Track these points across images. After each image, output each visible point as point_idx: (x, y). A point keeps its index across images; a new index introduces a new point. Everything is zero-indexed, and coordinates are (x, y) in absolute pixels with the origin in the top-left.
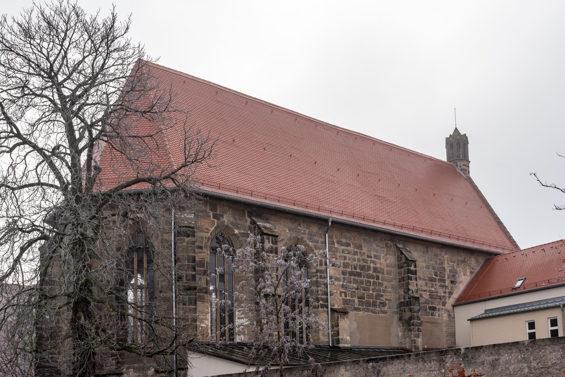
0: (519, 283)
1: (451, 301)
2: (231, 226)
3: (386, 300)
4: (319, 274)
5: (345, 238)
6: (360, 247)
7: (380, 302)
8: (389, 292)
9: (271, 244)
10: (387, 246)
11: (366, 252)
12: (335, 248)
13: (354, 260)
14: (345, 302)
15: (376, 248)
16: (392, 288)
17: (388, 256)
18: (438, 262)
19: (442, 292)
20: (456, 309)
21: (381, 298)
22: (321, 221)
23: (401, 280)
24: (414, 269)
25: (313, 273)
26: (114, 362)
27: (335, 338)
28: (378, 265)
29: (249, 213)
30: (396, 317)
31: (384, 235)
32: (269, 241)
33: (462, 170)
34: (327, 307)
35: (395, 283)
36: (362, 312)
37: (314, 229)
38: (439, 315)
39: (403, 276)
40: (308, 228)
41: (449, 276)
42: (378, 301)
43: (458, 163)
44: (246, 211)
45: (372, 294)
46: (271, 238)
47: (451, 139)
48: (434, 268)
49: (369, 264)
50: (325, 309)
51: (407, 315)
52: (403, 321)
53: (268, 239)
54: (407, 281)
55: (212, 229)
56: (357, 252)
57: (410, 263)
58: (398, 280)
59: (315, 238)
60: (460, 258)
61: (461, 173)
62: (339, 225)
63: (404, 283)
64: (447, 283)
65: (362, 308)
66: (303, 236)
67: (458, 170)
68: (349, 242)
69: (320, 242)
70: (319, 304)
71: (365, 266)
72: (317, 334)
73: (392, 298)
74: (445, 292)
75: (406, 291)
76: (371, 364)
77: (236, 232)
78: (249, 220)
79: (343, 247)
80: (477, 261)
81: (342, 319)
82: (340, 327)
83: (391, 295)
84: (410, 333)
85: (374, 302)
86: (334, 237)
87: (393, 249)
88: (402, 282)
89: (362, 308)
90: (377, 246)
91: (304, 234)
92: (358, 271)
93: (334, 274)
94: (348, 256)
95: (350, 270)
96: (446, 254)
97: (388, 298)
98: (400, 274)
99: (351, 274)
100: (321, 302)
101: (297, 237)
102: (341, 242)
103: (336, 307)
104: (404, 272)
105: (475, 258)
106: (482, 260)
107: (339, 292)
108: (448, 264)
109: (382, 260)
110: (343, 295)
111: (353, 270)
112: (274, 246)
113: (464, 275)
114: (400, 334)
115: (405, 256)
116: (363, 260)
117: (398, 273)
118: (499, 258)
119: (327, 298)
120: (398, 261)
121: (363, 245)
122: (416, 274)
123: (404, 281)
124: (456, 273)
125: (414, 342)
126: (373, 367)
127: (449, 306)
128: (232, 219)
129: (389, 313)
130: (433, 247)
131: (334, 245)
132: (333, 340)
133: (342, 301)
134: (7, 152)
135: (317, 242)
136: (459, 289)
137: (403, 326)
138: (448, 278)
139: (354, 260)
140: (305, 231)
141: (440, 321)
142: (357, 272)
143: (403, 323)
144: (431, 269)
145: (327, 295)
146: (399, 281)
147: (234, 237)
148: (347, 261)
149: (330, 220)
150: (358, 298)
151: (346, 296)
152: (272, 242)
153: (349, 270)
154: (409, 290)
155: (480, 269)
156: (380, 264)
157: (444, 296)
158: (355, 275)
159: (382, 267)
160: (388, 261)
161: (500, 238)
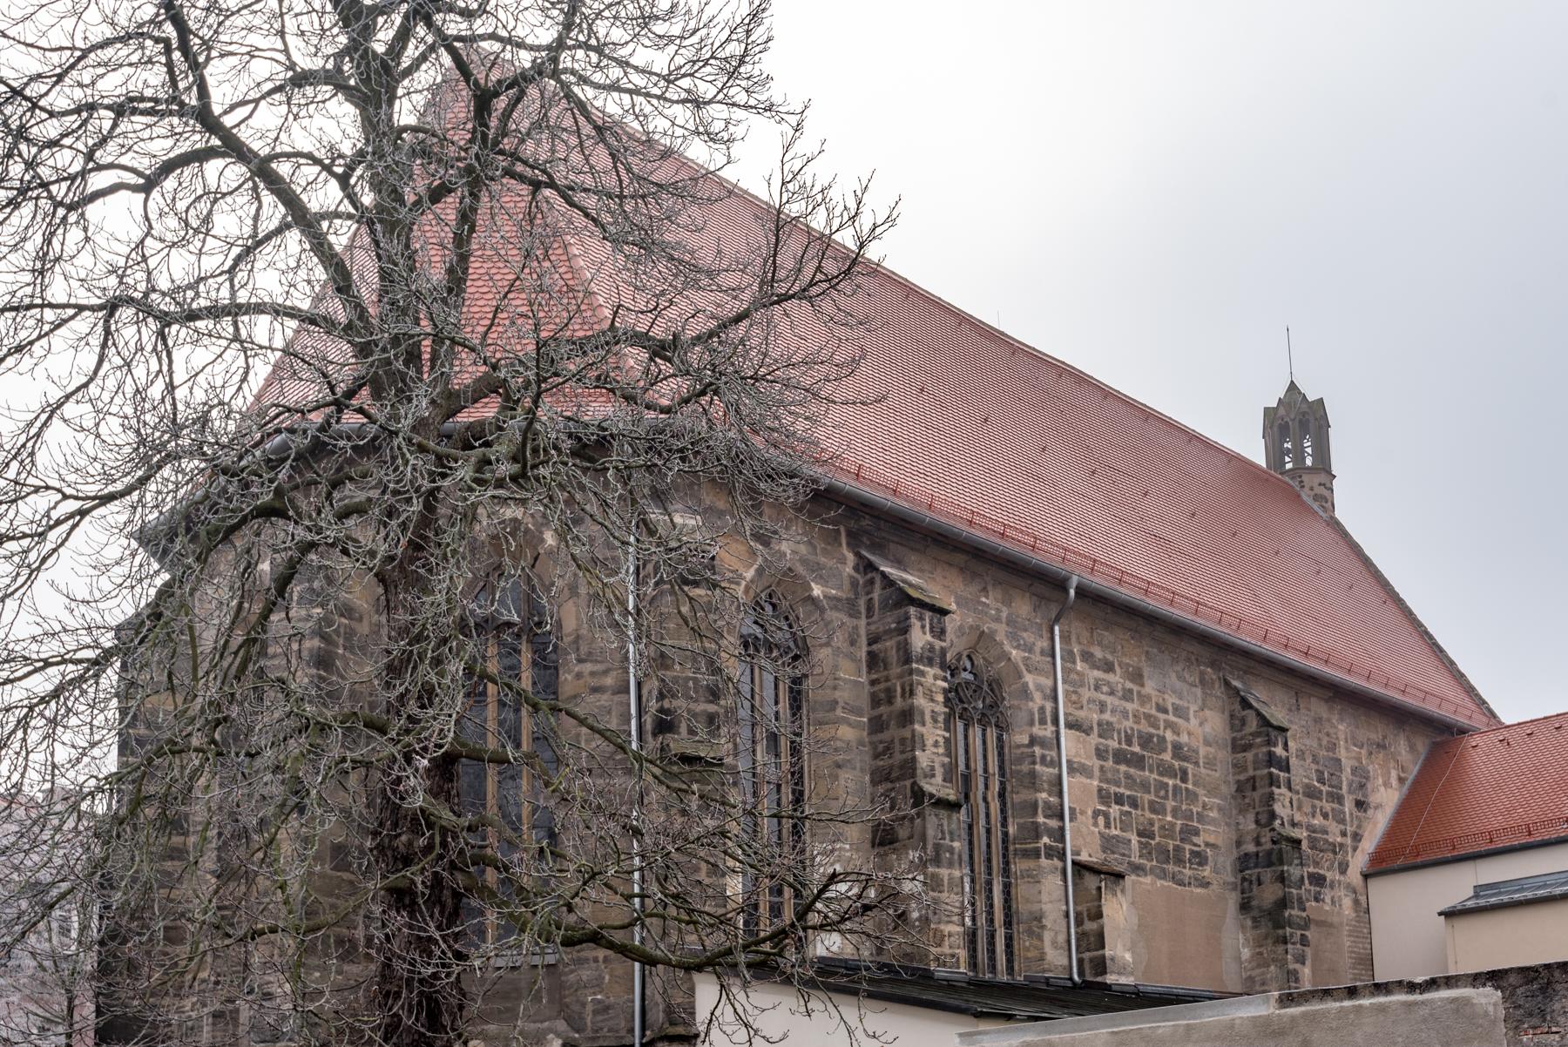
1: (1358, 861)
2: (800, 569)
3: (1207, 844)
4: (1037, 750)
5: (1100, 644)
6: (1137, 677)
7: (1192, 852)
8: (1213, 822)
9: (928, 637)
10: (1203, 682)
11: (1154, 693)
12: (1078, 673)
13: (1125, 714)
14: (1108, 844)
15: (1179, 685)
17: (1208, 713)
18: (1324, 743)
19: (1338, 832)
21: (1195, 840)
23: (1245, 787)
24: (1284, 754)
25: (1019, 746)
27: (1087, 955)
28: (1184, 739)
29: (850, 534)
30: (1233, 900)
31: (1196, 648)
32: (923, 627)
33: (1317, 498)
34: (1062, 856)
36: (1148, 880)
37: (1023, 607)
38: (1333, 902)
39: (1251, 773)
40: (1007, 602)
41: (1350, 785)
42: (1188, 847)
43: (1305, 478)
44: (842, 529)
45: (1173, 825)
46: (928, 615)
47: (1282, 412)
48: (1315, 760)
49: (1161, 732)
50: (1057, 862)
51: (1269, 894)
52: (1255, 913)
53: (921, 619)
54: (1267, 790)
55: (750, 574)
56: (1131, 691)
57: (1273, 733)
58: (1233, 788)
59: (1025, 635)
60: (1373, 736)
61: (1315, 506)
63: (1257, 795)
64: (1348, 806)
65: (1149, 865)
66: (994, 626)
67: (1306, 496)
68: (1110, 657)
69: (1037, 649)
70: (1041, 844)
71: (1151, 736)
72: (1035, 942)
73: (1219, 842)
74: (1344, 834)
75: (1264, 819)
77: (817, 591)
78: (850, 557)
79: (1097, 674)
80: (1412, 748)
81: (1109, 896)
82: (1105, 920)
83: (1218, 832)
84: (1281, 948)
85: (1177, 849)
86: (1074, 639)
87: (1218, 690)
89: (1149, 865)
90: (1179, 678)
91: (998, 620)
92: (1136, 749)
93: (1077, 755)
94: (1109, 700)
95: (1116, 745)
96: (1341, 720)
97: (1212, 840)
98: (1239, 767)
99: (1120, 757)
100: (1046, 840)
101: (978, 627)
103: (1084, 857)
104: (1255, 762)
105: (1408, 739)
106: (1422, 746)
107: (1090, 813)
109: (1194, 722)
110: (1101, 820)
111: (1124, 746)
112: (938, 644)
114: (1246, 953)
115: (1259, 714)
116: (1148, 717)
117: (1235, 766)
119: (1062, 829)
120: (1232, 727)
121: (1146, 672)
122: (1288, 770)
123: (1254, 789)
124: (1367, 778)
127: (1354, 875)
128: (803, 549)
129: (1215, 887)
130: (1310, 696)
131: (1074, 662)
132: (1080, 962)
133: (1098, 841)
134: (135, 189)
135: (1030, 650)
136: (1375, 825)
137: (1255, 927)
138: (1349, 792)
139: (1125, 716)
140: (998, 610)
141: (1335, 920)
142: (1133, 754)
143: (1254, 920)
144: (1309, 760)
145: (1061, 818)
147: (810, 607)
148: (1107, 716)
149: (1075, 580)
150: (1139, 835)
151: (1107, 826)
152: (932, 631)
153: (1113, 744)
154: (1273, 816)
155: (1420, 772)
156: (1189, 734)
157: (1341, 845)
158: (1128, 763)
159: (1194, 744)
160: (1207, 728)
161: (1442, 684)
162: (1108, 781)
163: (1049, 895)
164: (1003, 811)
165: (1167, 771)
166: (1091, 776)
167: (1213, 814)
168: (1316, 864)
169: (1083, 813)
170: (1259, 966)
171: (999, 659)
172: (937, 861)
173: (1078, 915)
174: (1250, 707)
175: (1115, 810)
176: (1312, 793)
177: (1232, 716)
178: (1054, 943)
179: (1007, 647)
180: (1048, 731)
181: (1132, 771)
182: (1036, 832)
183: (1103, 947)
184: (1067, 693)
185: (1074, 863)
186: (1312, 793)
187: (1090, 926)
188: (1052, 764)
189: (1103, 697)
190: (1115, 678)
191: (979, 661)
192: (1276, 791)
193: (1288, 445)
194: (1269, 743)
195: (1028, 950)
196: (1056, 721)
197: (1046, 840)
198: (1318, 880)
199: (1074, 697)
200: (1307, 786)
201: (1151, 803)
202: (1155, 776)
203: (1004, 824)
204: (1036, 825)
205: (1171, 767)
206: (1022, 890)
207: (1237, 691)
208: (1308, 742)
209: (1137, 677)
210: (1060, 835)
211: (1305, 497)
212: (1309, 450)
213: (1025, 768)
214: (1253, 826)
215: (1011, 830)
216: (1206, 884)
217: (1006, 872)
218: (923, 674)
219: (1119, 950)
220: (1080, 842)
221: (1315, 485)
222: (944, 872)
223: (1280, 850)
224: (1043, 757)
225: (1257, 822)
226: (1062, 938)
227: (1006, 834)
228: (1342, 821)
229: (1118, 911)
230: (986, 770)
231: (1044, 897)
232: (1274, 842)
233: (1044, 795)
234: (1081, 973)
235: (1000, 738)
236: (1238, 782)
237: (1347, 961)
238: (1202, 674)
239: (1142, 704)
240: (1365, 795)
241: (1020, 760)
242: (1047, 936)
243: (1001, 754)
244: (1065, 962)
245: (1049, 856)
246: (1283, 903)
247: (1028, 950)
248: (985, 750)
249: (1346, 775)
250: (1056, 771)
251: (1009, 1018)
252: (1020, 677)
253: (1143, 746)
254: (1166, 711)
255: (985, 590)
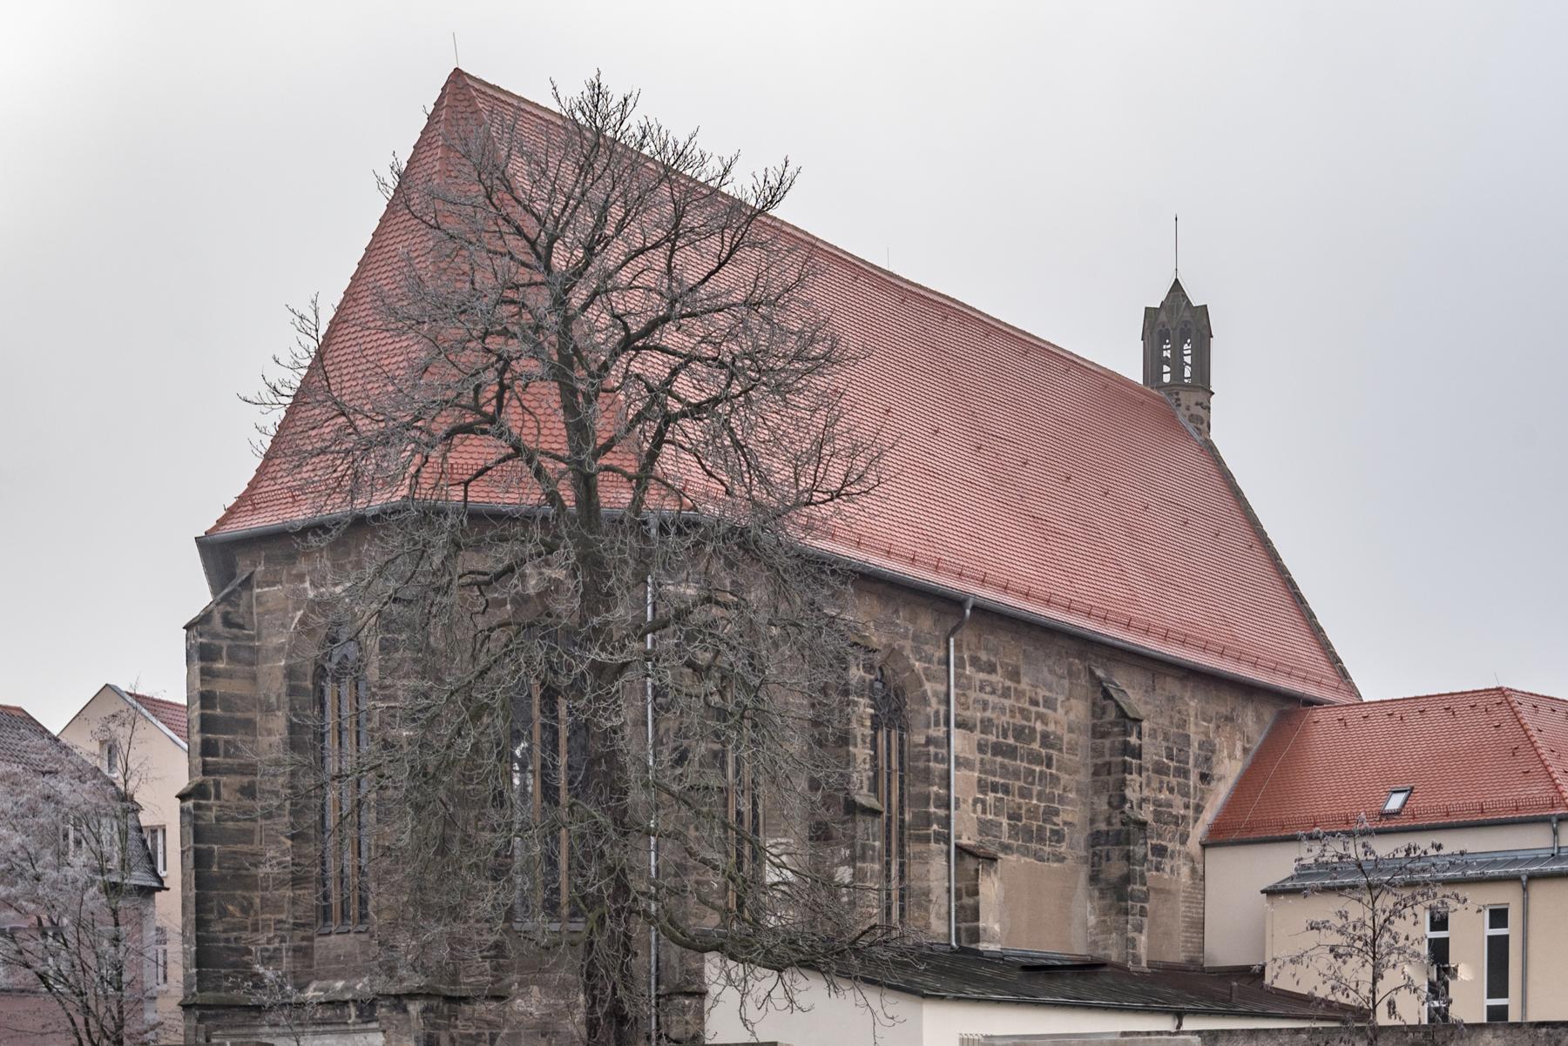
0: (1395, 802)
1: (1198, 832)
3: (1065, 823)
4: (932, 749)
5: (986, 649)
6: (1015, 675)
7: (1052, 831)
10: (1071, 674)
11: (1028, 688)
13: (1003, 710)
14: (985, 827)
15: (1049, 678)
16: (1078, 791)
20: (1210, 853)
21: (1055, 819)
22: (946, 604)
25: (917, 745)
26: (487, 964)
27: (963, 925)
28: (1051, 728)
30: (1083, 873)
33: (1192, 418)
34: (947, 841)
35: (1084, 777)
37: (926, 623)
38: (1172, 871)
39: (1107, 758)
40: (913, 621)
41: (1196, 760)
43: (1182, 395)
45: (1037, 807)
48: (1166, 739)
50: (943, 846)
51: (1115, 869)
52: (1102, 885)
54: (1120, 776)
57: (1129, 724)
58: (1091, 770)
59: (926, 647)
62: (991, 617)
63: (1111, 779)
64: (1194, 779)
66: (902, 642)
67: (1182, 417)
68: (993, 659)
69: (935, 659)
71: (1024, 727)
73: (1076, 821)
74: (1187, 807)
76: (1544, 1030)
79: (982, 676)
80: (1259, 719)
84: (1122, 919)
85: (1040, 829)
87: (1084, 680)
88: (1104, 777)
91: (905, 637)
92: (1011, 741)
93: (963, 750)
94: (991, 699)
96: (1193, 697)
97: (1069, 818)
98: (1097, 751)
99: (998, 749)
100: (935, 827)
102: (978, 659)
103: (964, 841)
106: (1269, 714)
108: (1196, 724)
109: (1060, 711)
110: (979, 807)
113: (1230, 757)
114: (1092, 920)
115: (1118, 705)
116: (1022, 710)
117: (1093, 750)
118: (1319, 714)
119: (948, 817)
120: (1094, 715)
122: (1140, 757)
123: (1109, 773)
124: (1213, 752)
125: (1132, 943)
126: (1547, 1034)
127: (1193, 845)
129: (1069, 862)
130: (1166, 675)
132: (958, 930)
135: (930, 661)
141: (1173, 887)
142: (1009, 745)
143: (1101, 891)
144: (1160, 738)
145: (948, 807)
146: (1095, 774)
148: (988, 714)
151: (984, 812)
153: (992, 738)
154: (1124, 799)
157: (1184, 817)
158: (1004, 754)
160: (1072, 716)
162: (986, 772)
163: (936, 873)
164: (901, 801)
165: (1034, 758)
166: (973, 770)
167: (1072, 795)
168: (1160, 836)
169: (965, 801)
170: (1103, 932)
171: (904, 670)
172: (863, 858)
173: (958, 890)
174: (1111, 697)
175: (990, 797)
176: (1160, 769)
177: (1094, 704)
178: (938, 915)
179: (912, 661)
180: (939, 732)
181: (1006, 761)
182: (927, 820)
183: (977, 919)
184: (957, 695)
185: (957, 846)
186: (1160, 769)
187: (967, 901)
188: (942, 761)
189: (986, 697)
190: (997, 678)
191: (887, 672)
192: (1128, 777)
193: (1167, 354)
194: (1126, 733)
195: (916, 919)
196: (947, 723)
197: (935, 827)
198: (1160, 851)
199: (963, 700)
200: (1157, 763)
201: (1021, 788)
202: (1025, 764)
203: (902, 813)
204: (928, 814)
205: (1039, 755)
206: (914, 869)
207: (1099, 681)
208: (1160, 721)
209: (1015, 675)
210: (946, 822)
211: (1180, 418)
212: (1188, 359)
213: (921, 764)
214: (1106, 807)
215: (907, 817)
216: (1061, 859)
217: (901, 853)
218: (856, 704)
219: (990, 922)
220: (962, 827)
221: (1192, 404)
222: (867, 866)
223: (1128, 833)
224: (936, 755)
225: (1110, 804)
226: (944, 910)
227: (902, 821)
228: (1187, 795)
229: (990, 889)
230: (889, 767)
231: (932, 876)
232: (1123, 824)
233: (935, 788)
234: (958, 940)
235: (901, 739)
236: (1095, 765)
237: (1180, 925)
238: (1071, 665)
239: (1018, 699)
240: (1210, 768)
241: (917, 758)
242: (933, 909)
243: (901, 752)
244: (945, 930)
245: (937, 841)
246: (1127, 879)
247: (916, 919)
248: (889, 749)
249: (1194, 749)
250: (944, 766)
251: (943, 998)
252: (921, 685)
253: (1016, 738)
254: (1036, 703)
255: (896, 611)
